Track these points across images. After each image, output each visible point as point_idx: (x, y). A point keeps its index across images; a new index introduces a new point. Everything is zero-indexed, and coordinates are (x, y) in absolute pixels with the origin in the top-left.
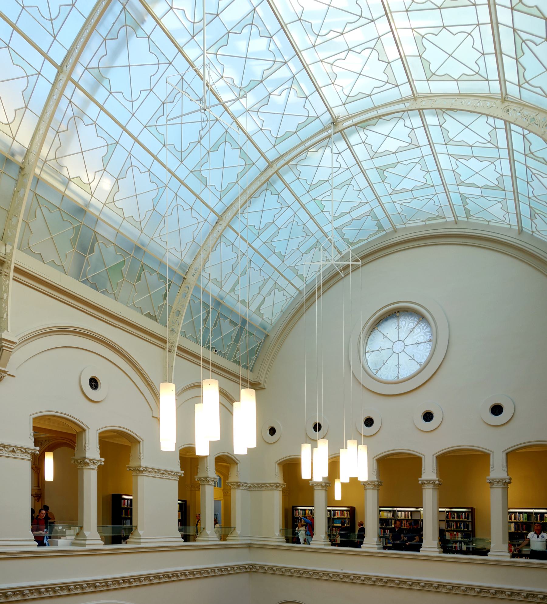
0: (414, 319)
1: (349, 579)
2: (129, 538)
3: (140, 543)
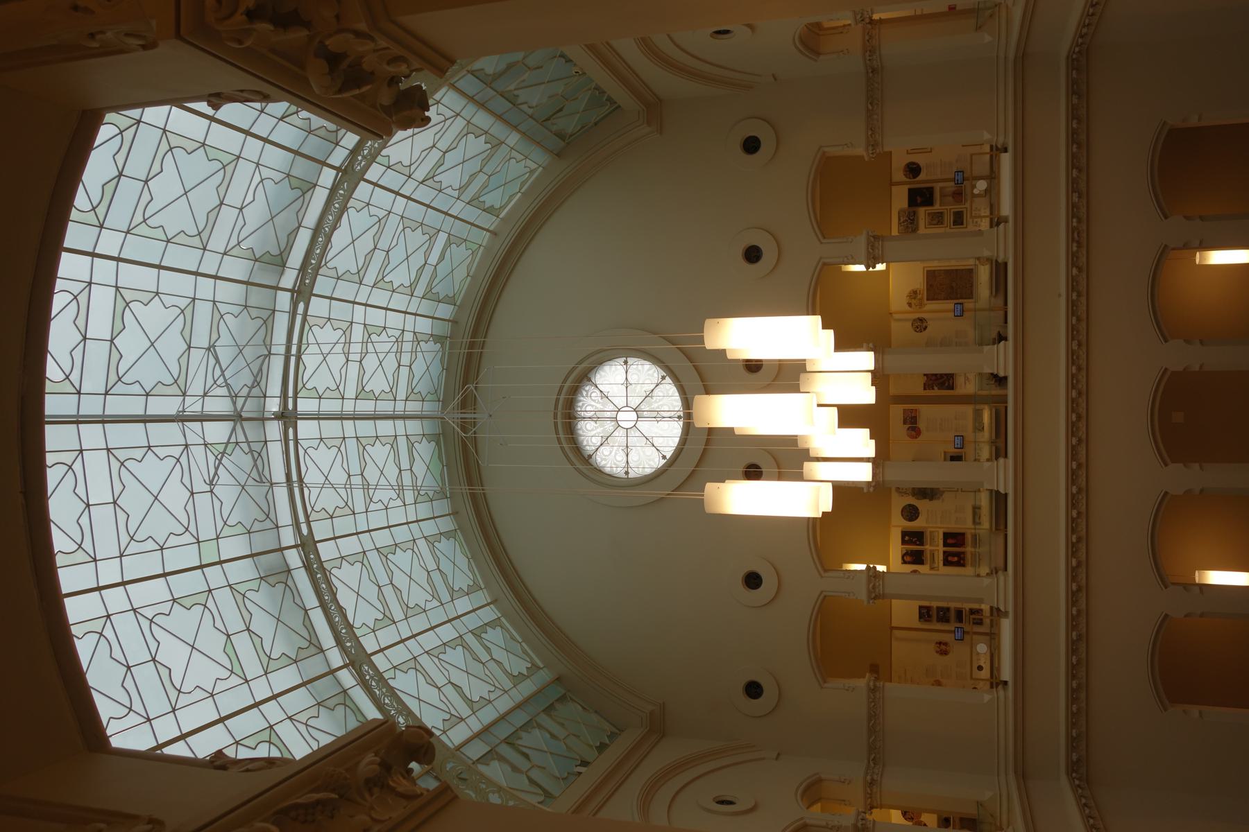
0: (601, 375)
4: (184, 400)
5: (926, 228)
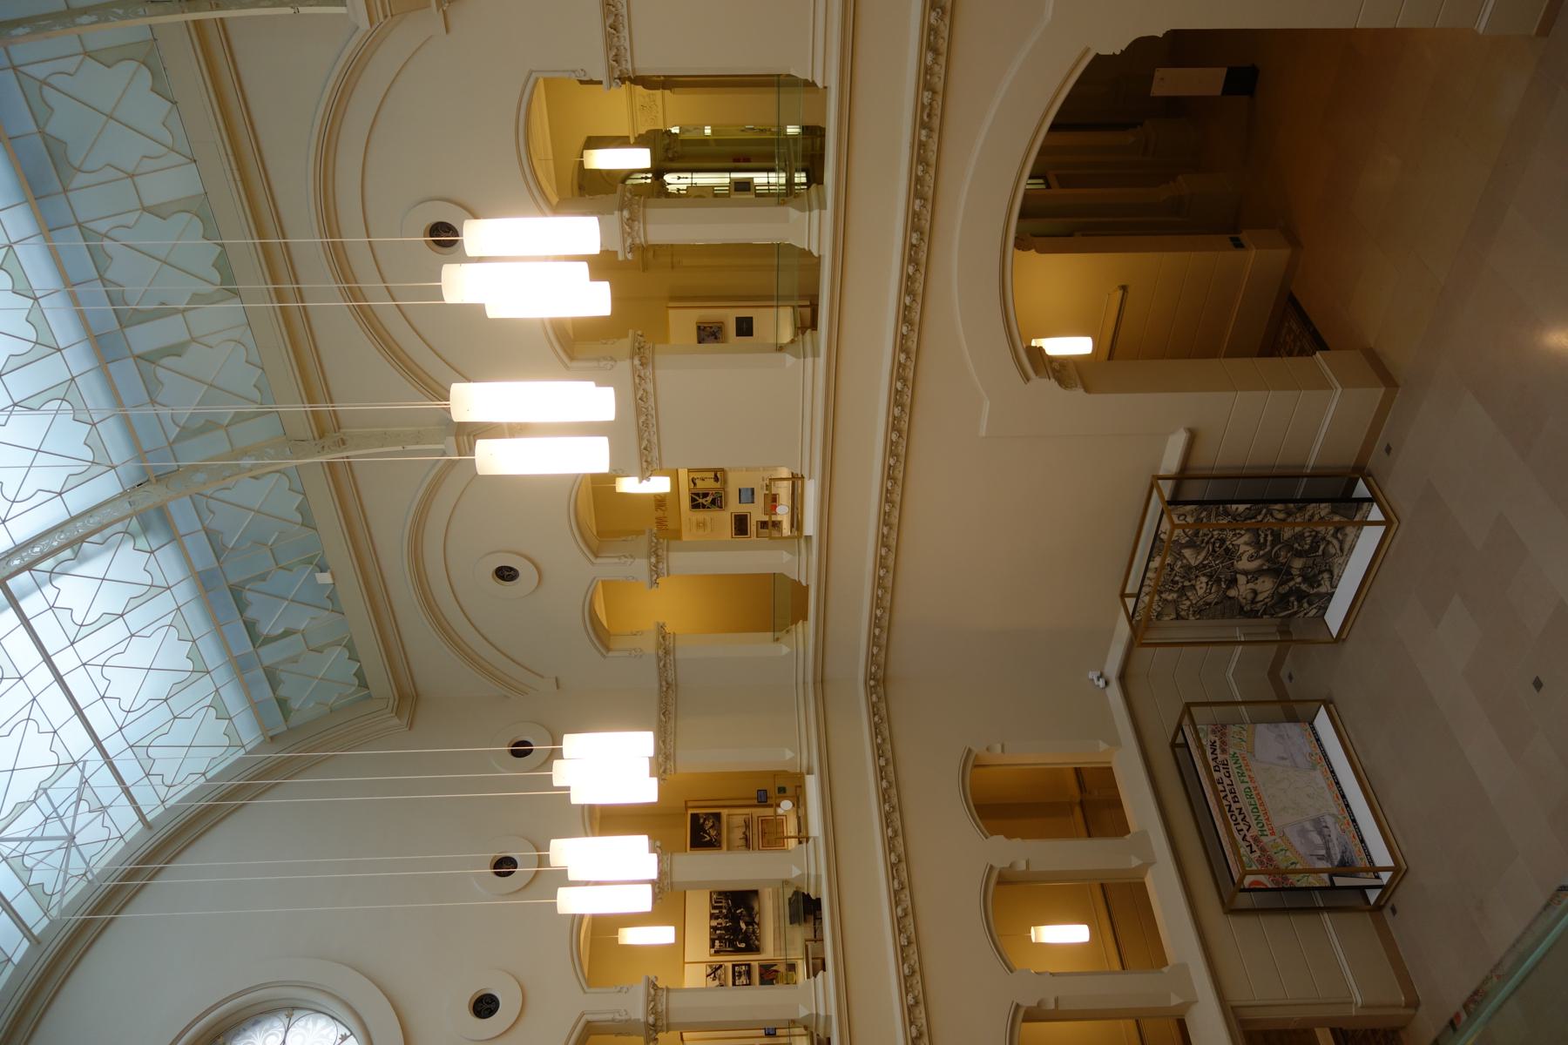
0: (306, 1024)
1: (915, 305)
2: (808, 894)
3: (818, 877)
4: (15, 243)
5: (758, 817)
